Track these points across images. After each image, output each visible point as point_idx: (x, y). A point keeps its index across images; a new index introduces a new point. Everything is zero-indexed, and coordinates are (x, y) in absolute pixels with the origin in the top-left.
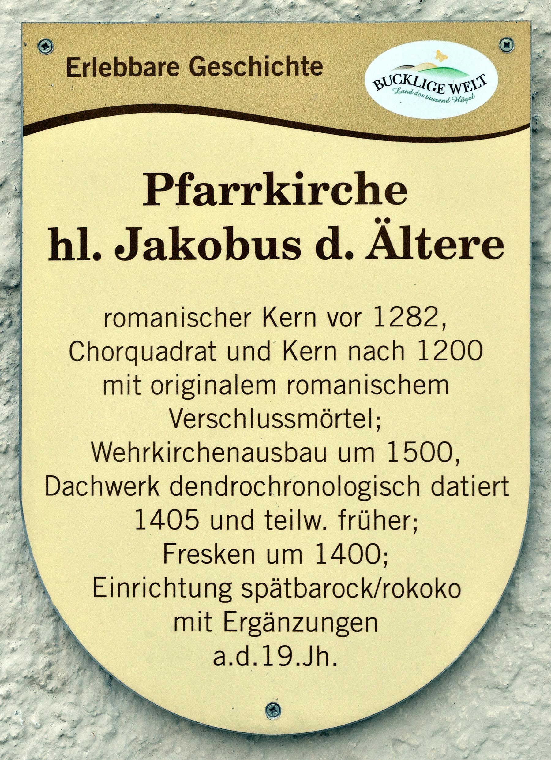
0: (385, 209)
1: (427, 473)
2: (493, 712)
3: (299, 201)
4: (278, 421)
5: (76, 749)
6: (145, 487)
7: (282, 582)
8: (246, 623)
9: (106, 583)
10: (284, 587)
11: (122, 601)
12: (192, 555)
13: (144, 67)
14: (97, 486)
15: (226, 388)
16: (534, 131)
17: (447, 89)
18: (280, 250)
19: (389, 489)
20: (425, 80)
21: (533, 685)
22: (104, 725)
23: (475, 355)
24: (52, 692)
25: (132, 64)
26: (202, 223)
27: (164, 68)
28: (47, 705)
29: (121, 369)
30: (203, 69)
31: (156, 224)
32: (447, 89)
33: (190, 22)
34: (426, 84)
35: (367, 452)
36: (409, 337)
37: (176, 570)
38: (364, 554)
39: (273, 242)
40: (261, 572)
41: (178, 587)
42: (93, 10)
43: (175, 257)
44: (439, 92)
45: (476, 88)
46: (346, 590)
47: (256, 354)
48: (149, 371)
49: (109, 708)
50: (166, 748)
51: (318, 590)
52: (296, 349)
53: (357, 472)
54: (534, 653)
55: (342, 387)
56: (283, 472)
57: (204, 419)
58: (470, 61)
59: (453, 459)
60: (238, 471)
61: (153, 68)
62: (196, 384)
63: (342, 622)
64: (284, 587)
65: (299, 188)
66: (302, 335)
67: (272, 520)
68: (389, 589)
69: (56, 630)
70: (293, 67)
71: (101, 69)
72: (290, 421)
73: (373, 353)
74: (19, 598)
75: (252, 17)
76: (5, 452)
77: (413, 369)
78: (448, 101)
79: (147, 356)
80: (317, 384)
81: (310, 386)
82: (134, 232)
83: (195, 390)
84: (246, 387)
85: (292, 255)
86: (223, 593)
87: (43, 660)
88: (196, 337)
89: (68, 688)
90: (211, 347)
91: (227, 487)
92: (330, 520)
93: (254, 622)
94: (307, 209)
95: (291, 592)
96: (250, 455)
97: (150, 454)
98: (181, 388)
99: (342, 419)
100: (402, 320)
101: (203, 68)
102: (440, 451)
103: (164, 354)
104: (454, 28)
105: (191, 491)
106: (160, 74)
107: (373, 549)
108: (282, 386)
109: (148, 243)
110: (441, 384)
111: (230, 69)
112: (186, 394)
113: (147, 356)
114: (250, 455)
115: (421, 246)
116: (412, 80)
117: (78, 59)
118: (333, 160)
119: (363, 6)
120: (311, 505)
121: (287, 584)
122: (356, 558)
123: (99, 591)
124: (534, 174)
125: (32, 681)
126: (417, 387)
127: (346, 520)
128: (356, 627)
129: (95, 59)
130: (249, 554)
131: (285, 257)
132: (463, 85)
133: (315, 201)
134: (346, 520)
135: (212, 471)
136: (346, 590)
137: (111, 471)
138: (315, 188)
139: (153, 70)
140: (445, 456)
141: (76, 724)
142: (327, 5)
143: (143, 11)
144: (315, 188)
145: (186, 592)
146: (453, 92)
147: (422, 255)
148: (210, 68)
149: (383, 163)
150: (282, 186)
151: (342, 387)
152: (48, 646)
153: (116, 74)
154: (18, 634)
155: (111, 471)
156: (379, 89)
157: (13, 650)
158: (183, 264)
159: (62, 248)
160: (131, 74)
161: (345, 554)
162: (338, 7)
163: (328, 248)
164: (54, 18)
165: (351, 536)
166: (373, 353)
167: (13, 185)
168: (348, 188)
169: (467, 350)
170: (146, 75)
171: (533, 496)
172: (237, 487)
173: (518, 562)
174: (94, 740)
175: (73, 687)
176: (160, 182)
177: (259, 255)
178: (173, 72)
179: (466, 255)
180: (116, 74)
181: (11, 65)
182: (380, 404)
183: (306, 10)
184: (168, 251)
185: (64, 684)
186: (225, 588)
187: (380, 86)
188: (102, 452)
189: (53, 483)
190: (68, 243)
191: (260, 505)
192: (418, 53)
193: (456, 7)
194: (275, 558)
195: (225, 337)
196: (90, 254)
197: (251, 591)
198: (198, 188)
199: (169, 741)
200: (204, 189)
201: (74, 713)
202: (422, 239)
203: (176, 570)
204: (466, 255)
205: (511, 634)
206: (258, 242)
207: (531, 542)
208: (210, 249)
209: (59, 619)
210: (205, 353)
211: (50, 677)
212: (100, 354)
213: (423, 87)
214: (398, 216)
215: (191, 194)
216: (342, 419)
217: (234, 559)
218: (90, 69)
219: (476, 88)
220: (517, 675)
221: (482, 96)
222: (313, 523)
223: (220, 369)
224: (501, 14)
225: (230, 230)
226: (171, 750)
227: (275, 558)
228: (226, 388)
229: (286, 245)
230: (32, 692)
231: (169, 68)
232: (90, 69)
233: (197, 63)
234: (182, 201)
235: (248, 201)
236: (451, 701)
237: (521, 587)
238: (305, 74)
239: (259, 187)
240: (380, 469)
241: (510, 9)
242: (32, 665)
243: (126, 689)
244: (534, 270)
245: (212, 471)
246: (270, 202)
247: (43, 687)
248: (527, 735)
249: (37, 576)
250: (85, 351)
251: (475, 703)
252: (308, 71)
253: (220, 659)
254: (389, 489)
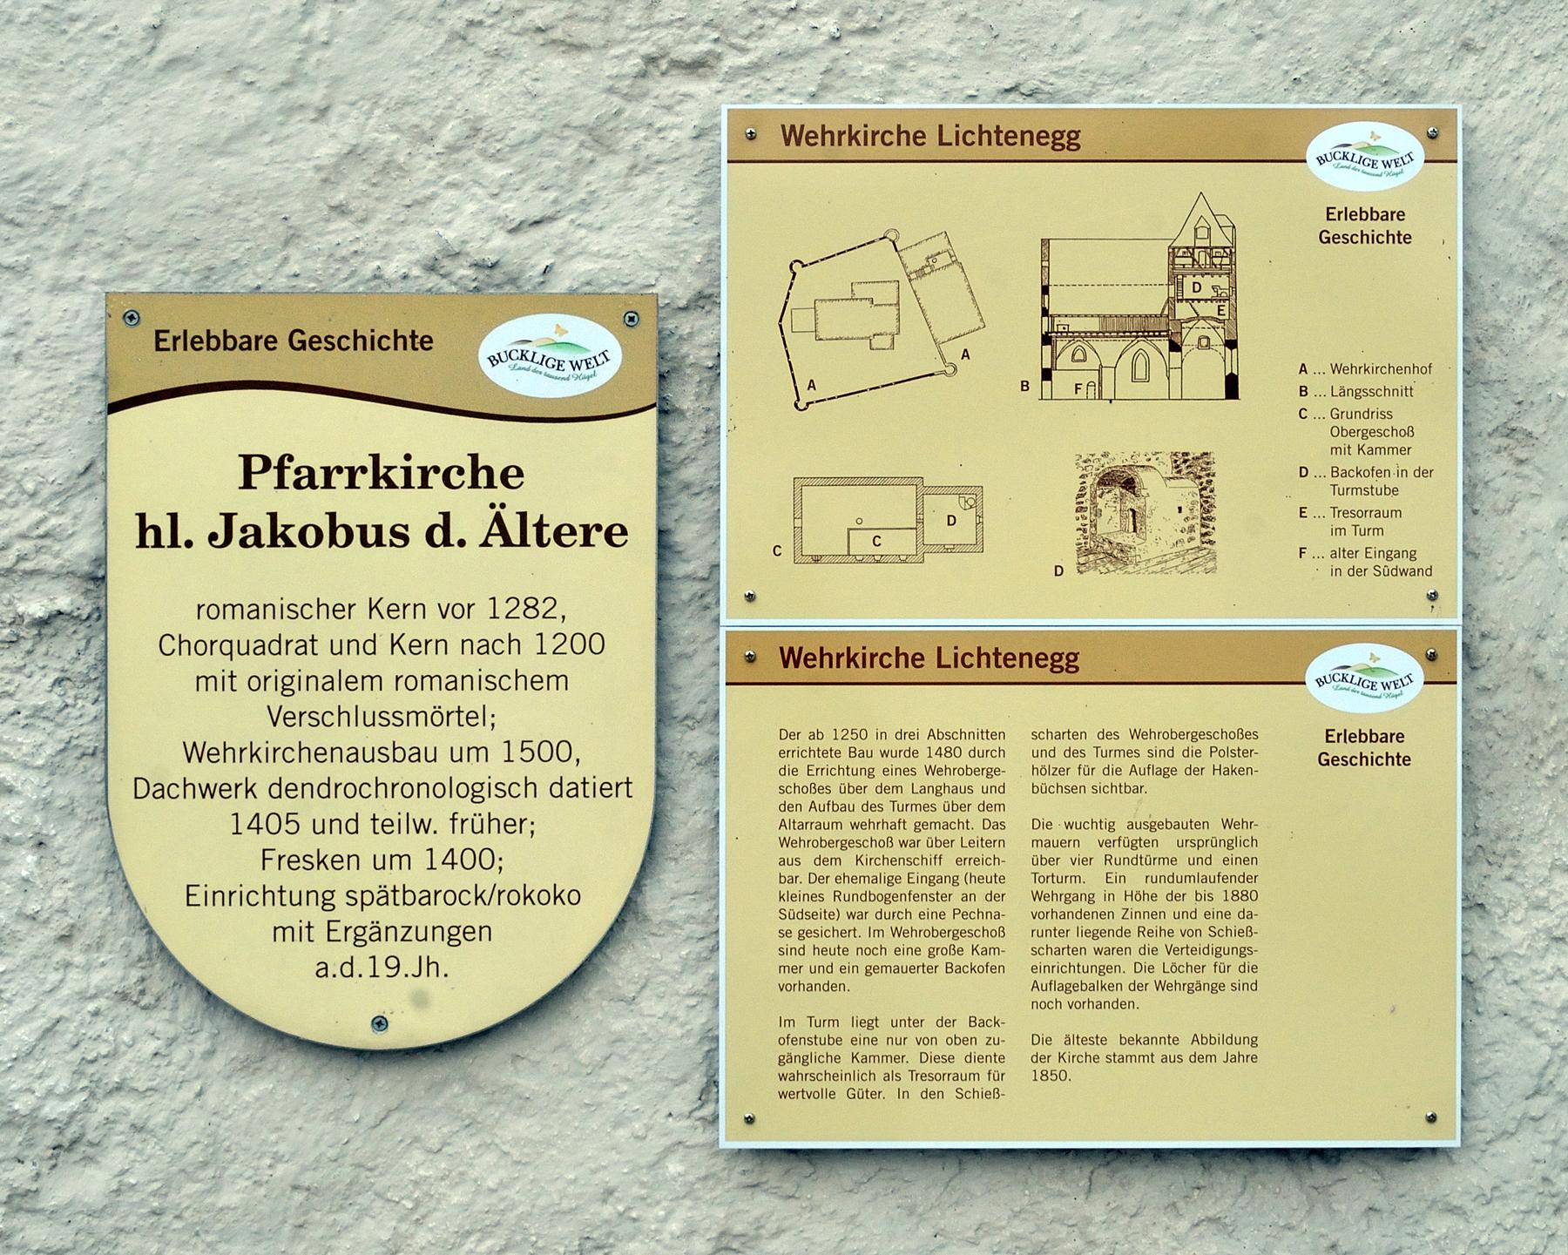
0: (500, 493)
1: (543, 774)
2: (618, 1026)
3: (408, 485)
4: (384, 718)
5: (172, 1068)
6: (242, 790)
7: (389, 889)
8: (351, 933)
9: (200, 891)
10: (391, 895)
11: (216, 912)
12: (292, 861)
13: (239, 341)
14: (189, 789)
15: (329, 684)
16: (663, 413)
18: (387, 536)
19: (505, 791)
21: (661, 997)
22: (202, 1044)
23: (596, 648)
24: (145, 1008)
25: (226, 337)
26: (303, 508)
27: (261, 342)
28: (139, 1022)
29: (215, 664)
30: (304, 343)
31: (253, 509)
33: (291, 293)
34: (544, 361)
35: (481, 752)
36: (525, 629)
37: (275, 877)
38: (477, 859)
39: (379, 528)
40: (366, 879)
41: (277, 895)
42: (187, 280)
43: (274, 544)
46: (458, 898)
47: (361, 648)
48: (246, 666)
49: (207, 1024)
50: (269, 1067)
51: (429, 898)
52: (405, 643)
53: (470, 772)
54: (661, 964)
55: (454, 683)
56: (390, 773)
57: (305, 716)
58: (595, 337)
59: (573, 758)
60: (341, 772)
61: (249, 342)
62: (296, 680)
63: (454, 931)
64: (391, 895)
65: (407, 470)
66: (411, 628)
67: (378, 824)
68: (504, 896)
69: (149, 942)
70: (400, 341)
71: (193, 343)
72: (398, 719)
73: (487, 647)
74: (109, 910)
75: (361, 289)
76: (93, 754)
77: (531, 664)
79: (243, 650)
80: (229, 609)
81: (420, 682)
82: (229, 518)
83: (295, 686)
84: (350, 682)
85: (400, 542)
86: (326, 903)
87: (135, 974)
88: (296, 630)
89: (163, 1003)
90: (313, 640)
91: (330, 789)
92: (441, 824)
93: (360, 931)
94: (416, 493)
95: (399, 900)
96: (355, 755)
97: (246, 754)
98: (280, 684)
99: (454, 717)
100: (519, 612)
101: (303, 342)
102: (558, 750)
103: (262, 648)
104: (582, 301)
105: (291, 794)
107: (487, 854)
108: (389, 682)
109: (244, 530)
110: (561, 680)
111: (333, 344)
112: (286, 690)
113: (243, 650)
114: (355, 755)
115: (535, 532)
116: (529, 356)
118: (442, 441)
119: (481, 277)
120: (420, 808)
121: (395, 891)
122: (468, 864)
123: (192, 900)
124: (661, 458)
125: (123, 996)
126: (534, 682)
127: (458, 823)
128: (469, 936)
130: (353, 860)
131: (392, 544)
133: (425, 485)
134: (458, 823)
135: (314, 772)
136: (458, 898)
137: (203, 773)
138: (425, 472)
139: (248, 344)
140: (564, 756)
141: (171, 1042)
142: (443, 276)
143: (242, 281)
144: (425, 472)
145: (286, 900)
147: (540, 543)
148: (311, 342)
149: (498, 444)
150: (389, 468)
151: (454, 683)
152: (140, 960)
153: (209, 348)
154: (107, 947)
155: (203, 773)
157: (103, 964)
158: (282, 551)
159: (150, 534)
160: (225, 348)
161: (457, 860)
162: (454, 279)
163: (438, 535)
164: (145, 288)
165: (461, 841)
166: (487, 647)
167: (100, 467)
168: (461, 472)
169: (587, 643)
171: (658, 800)
172: (341, 788)
173: (643, 866)
174: (192, 1058)
175: (168, 1002)
176: (257, 464)
177: (364, 543)
179: (587, 542)
180: (209, 348)
181: (97, 339)
182: (494, 701)
183: (420, 281)
184: (266, 538)
185: (158, 1000)
186: (328, 895)
188: (194, 752)
189: (142, 785)
190: (157, 530)
191: (366, 808)
192: (536, 327)
193: (582, 279)
194: (380, 864)
195: (327, 630)
196: (181, 542)
197: (357, 899)
198: (298, 471)
199: (272, 1059)
200: (305, 472)
201: (171, 1031)
202: (540, 526)
203: (275, 877)
204: (587, 542)
205: (637, 944)
206: (363, 528)
207: (658, 847)
208: (311, 536)
209: (151, 932)
210: (307, 646)
211: (143, 992)
212: (193, 648)
214: (514, 501)
215: (290, 477)
216: (454, 717)
217: (337, 865)
218: (180, 343)
220: (643, 987)
221: (606, 373)
222: (423, 826)
223: (323, 664)
224: (630, 287)
225: (332, 516)
226: (276, 1068)
227: (380, 864)
228: (329, 684)
229: (393, 532)
230: (123, 1009)
231: (266, 342)
232: (180, 343)
233: (297, 336)
234: (281, 485)
235: (352, 484)
236: (574, 1014)
237: (648, 894)
238: (414, 349)
239: (364, 470)
240: (495, 770)
241: (640, 281)
242: (123, 979)
243: (226, 1006)
244: (661, 558)
245: (314, 772)
246: (376, 485)
247: (136, 1003)
248: (654, 1049)
249: (127, 887)
250: (175, 645)
251: (599, 1016)
252: (418, 346)
253: (323, 970)
254: (505, 791)
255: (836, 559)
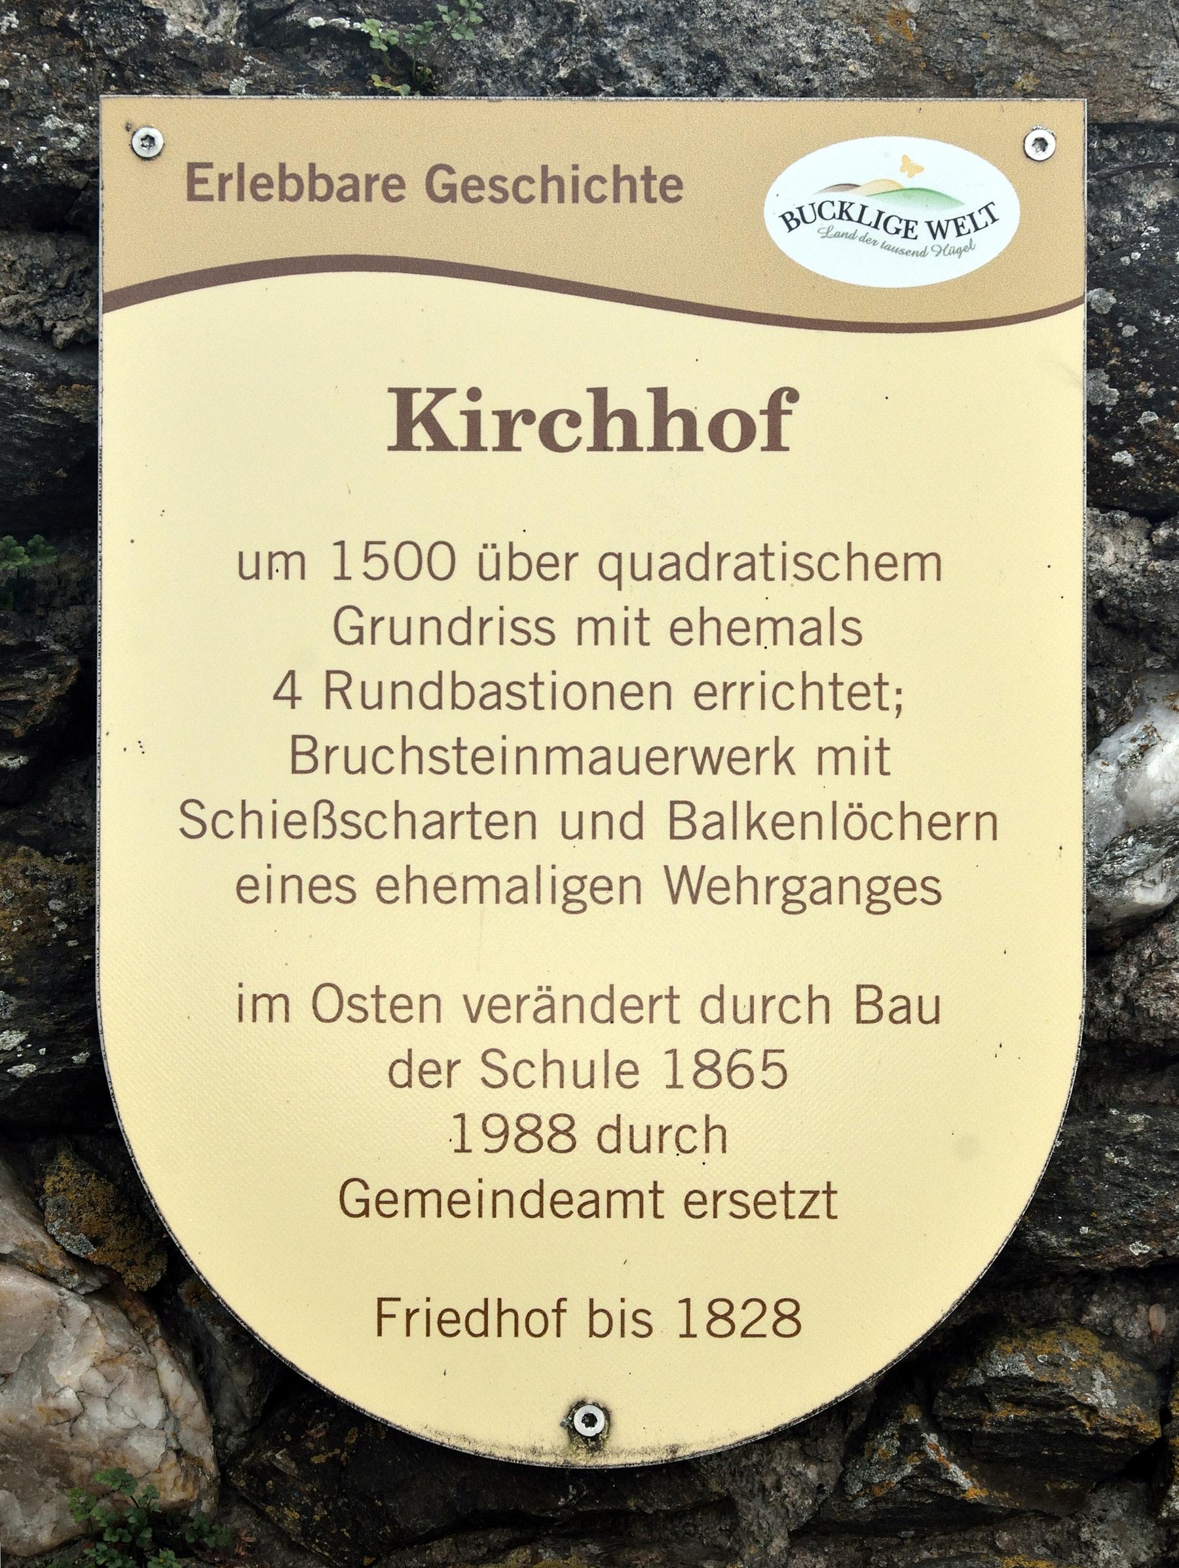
3: (474, 443)
13: (338, 184)
17: (922, 231)
20: (881, 213)
25: (313, 177)
27: (377, 187)
32: (922, 231)
34: (882, 221)
41: (828, 691)
44: (906, 236)
45: (977, 229)
61: (355, 186)
65: (473, 419)
70: (625, 186)
71: (254, 186)
78: (923, 254)
94: (490, 461)
99: (464, 822)
101: (451, 187)
106: (369, 198)
111: (504, 190)
116: (854, 212)
117: (209, 165)
129: (241, 167)
132: (952, 223)
138: (506, 420)
139: (353, 189)
144: (506, 420)
146: (934, 236)
148: (465, 188)
153: (283, 196)
156: (791, 229)
160: (313, 196)
168: (574, 420)
170: (341, 198)
178: (394, 193)
180: (283, 196)
187: (793, 224)
208: (732, 431)
213: (876, 227)
216: (464, 822)
218: (232, 187)
219: (977, 229)
221: (991, 244)
231: (386, 188)
232: (232, 187)
233: (441, 177)
238: (650, 199)
255: (859, 997)
